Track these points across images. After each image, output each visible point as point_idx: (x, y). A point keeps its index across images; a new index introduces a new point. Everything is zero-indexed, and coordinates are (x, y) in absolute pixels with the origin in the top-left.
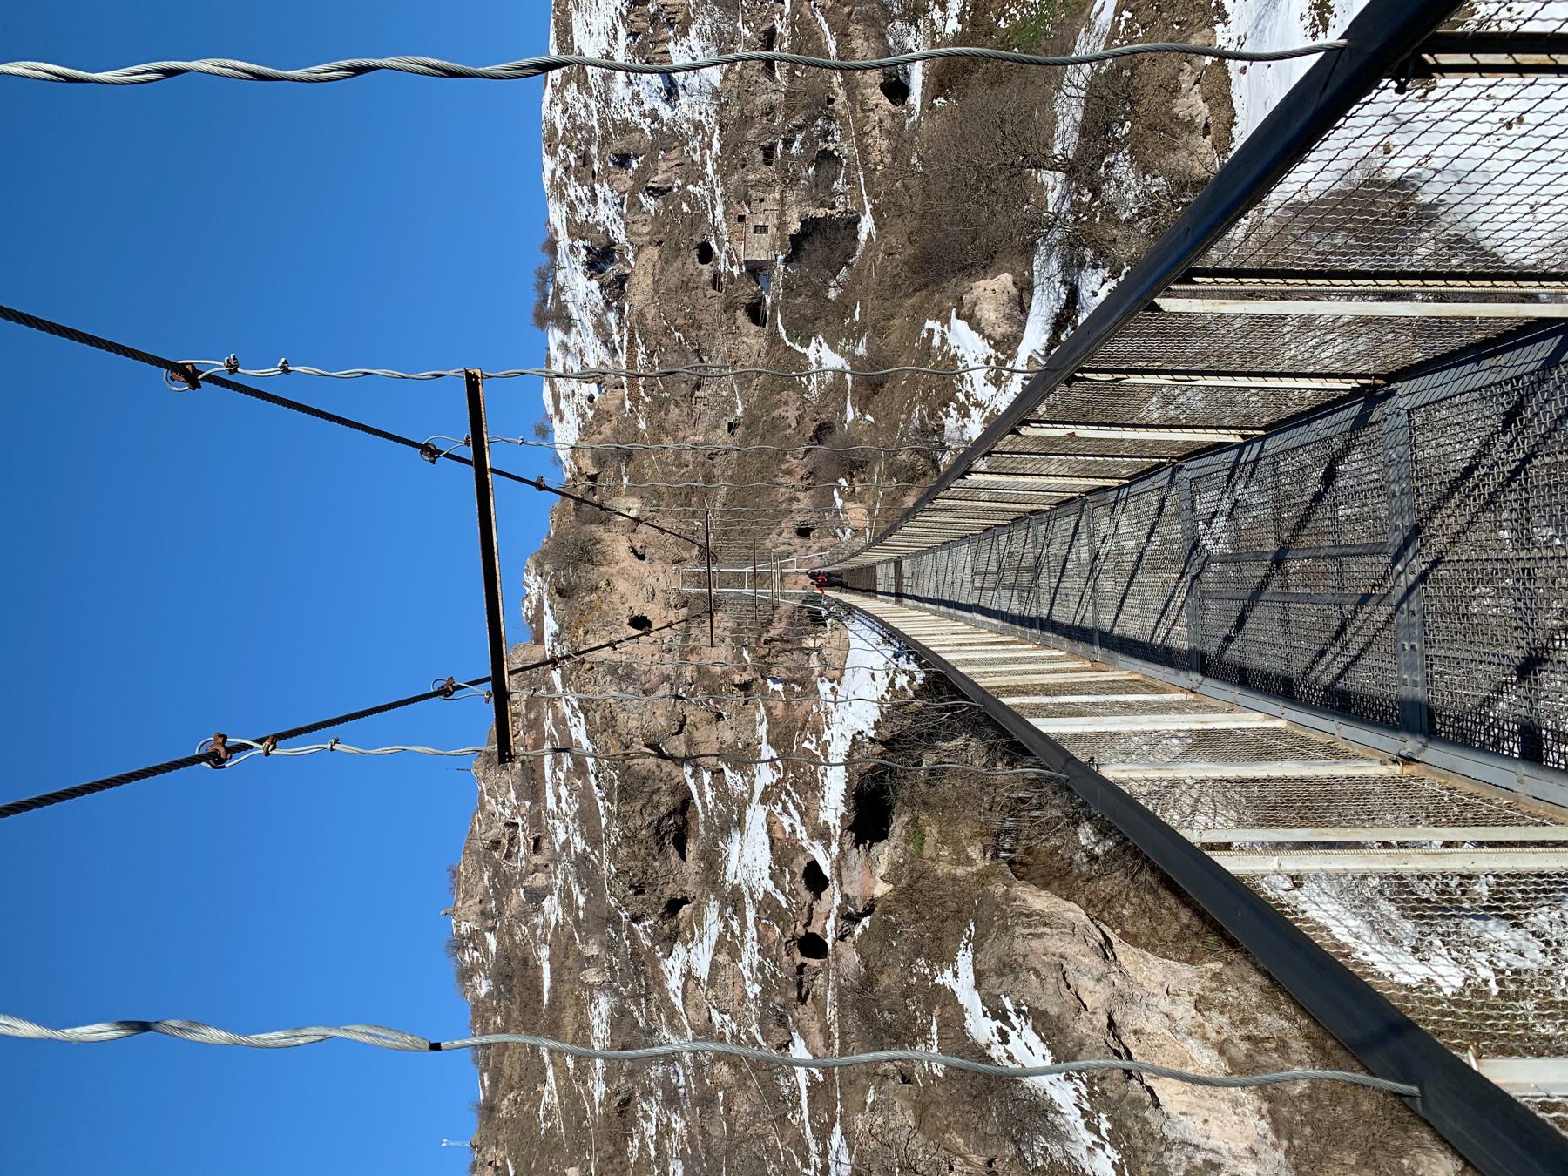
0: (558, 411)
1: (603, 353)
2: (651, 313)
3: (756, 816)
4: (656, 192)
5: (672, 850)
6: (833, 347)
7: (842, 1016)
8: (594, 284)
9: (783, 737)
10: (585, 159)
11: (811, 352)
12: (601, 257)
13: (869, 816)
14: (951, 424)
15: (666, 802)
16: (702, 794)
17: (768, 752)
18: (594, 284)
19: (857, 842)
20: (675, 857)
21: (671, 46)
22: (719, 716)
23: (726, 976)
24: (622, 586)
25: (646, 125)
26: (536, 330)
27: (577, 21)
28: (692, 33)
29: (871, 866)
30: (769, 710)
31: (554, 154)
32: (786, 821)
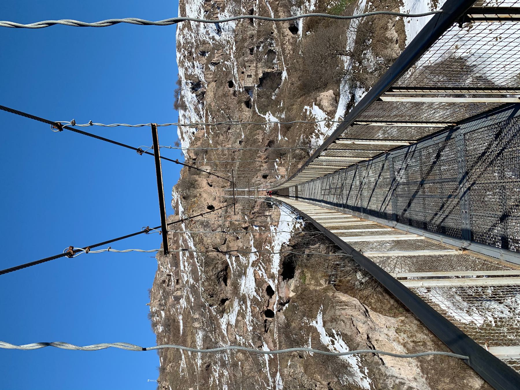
0: (183, 138)
1: (197, 118)
2: (213, 104)
3: (250, 271)
4: (214, 64)
5: (222, 283)
6: (274, 115)
7: (279, 337)
8: (194, 95)
9: (259, 245)
10: (191, 53)
11: (266, 117)
12: (196, 86)
13: (288, 270)
14: (313, 140)
15: (220, 267)
16: (232, 264)
17: (254, 250)
18: (194, 95)
19: (284, 279)
20: (223, 285)
21: (219, 15)
22: (238, 238)
23: (241, 324)
24: (205, 195)
25: (211, 42)
26: (175, 110)
27: (187, 7)
28: (226, 11)
29: (288, 287)
30: (254, 236)
31: (180, 52)
32: (260, 272)
